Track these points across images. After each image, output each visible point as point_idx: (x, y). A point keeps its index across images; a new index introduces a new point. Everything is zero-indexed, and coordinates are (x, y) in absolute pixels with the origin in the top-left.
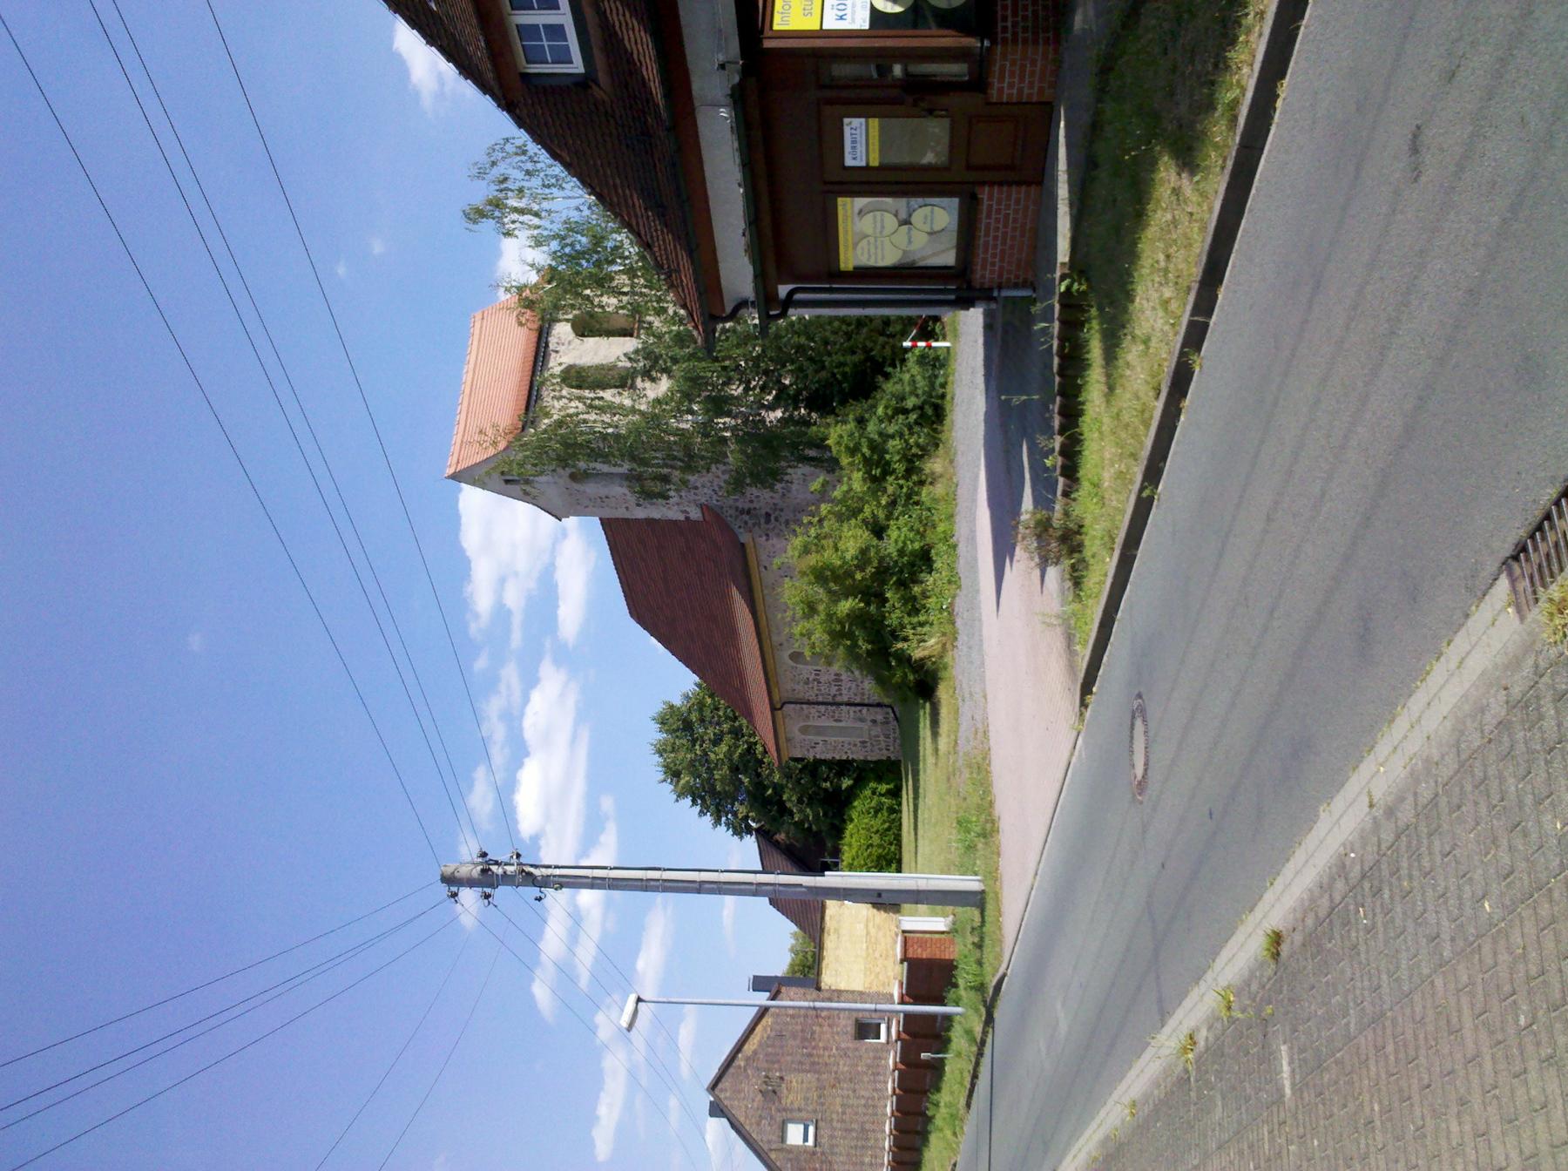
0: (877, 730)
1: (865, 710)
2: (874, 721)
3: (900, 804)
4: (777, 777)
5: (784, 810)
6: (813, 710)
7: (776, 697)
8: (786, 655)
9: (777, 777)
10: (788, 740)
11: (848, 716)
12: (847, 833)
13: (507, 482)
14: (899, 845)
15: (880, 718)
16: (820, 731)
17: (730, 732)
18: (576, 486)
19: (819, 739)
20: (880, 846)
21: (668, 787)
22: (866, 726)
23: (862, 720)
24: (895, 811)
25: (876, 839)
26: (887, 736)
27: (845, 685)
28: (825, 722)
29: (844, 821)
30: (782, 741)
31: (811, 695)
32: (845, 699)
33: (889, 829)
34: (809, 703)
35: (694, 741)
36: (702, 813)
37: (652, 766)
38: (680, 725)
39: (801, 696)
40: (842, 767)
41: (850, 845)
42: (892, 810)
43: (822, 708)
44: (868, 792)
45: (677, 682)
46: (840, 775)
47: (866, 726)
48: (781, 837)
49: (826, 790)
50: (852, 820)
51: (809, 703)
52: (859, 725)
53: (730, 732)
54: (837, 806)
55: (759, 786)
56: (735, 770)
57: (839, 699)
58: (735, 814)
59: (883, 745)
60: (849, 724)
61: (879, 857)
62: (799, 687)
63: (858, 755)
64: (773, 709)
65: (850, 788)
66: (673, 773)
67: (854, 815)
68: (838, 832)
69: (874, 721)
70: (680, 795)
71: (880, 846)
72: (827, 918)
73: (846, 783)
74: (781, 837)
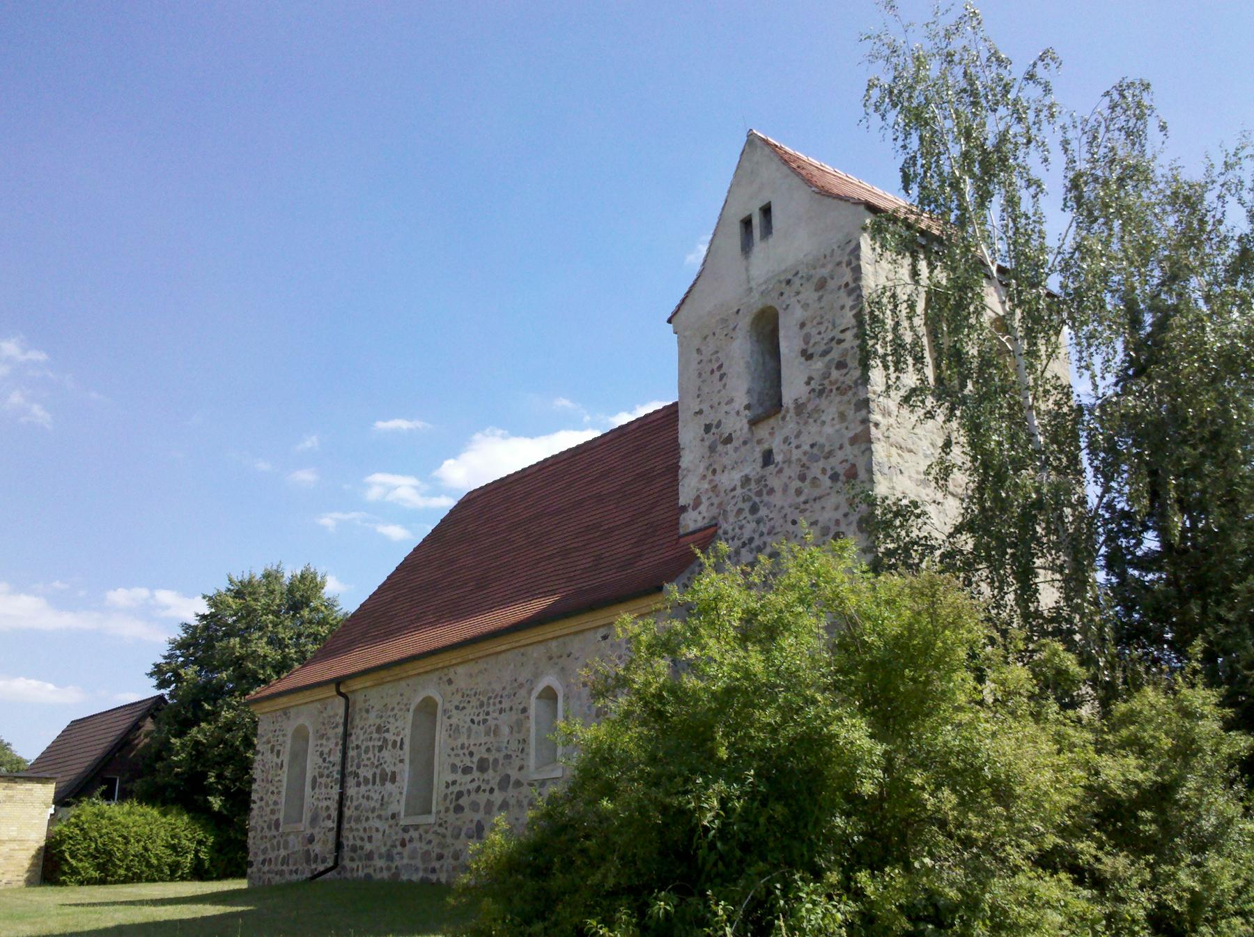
0: (296, 844)
1: (331, 824)
2: (311, 840)
3: (183, 878)
4: (227, 714)
5: (183, 727)
6: (332, 745)
7: (356, 685)
8: (432, 692)
9: (227, 714)
10: (285, 711)
11: (321, 798)
12: (148, 809)
13: (747, 223)
14: (126, 880)
15: (317, 848)
16: (298, 756)
17: (284, 657)
18: (745, 322)
19: (285, 757)
20: (125, 854)
21: (223, 586)
22: (304, 826)
23: (314, 820)
24: (174, 873)
25: (134, 848)
26: (285, 861)
27: (375, 792)
28: (312, 762)
29: (164, 803)
30: (283, 702)
31: (358, 737)
32: (351, 791)
33: (149, 865)
34: (346, 735)
35: (276, 614)
36: (186, 627)
37: (251, 567)
38: (300, 596)
39: (357, 721)
40: (240, 800)
41: (129, 814)
42: (175, 867)
43: (336, 757)
44: (200, 835)
45: (346, 591)
46: (226, 793)
47: (304, 826)
48: (149, 725)
49: (205, 776)
50: (165, 815)
51: (346, 735)
52: (307, 816)
53: (284, 657)
54: (181, 794)
55: (215, 692)
56: (238, 662)
57: (351, 781)
58: (184, 665)
59: (272, 855)
60: (308, 800)
61: (110, 854)
62: (372, 719)
63: (257, 818)
64: (338, 682)
65: (208, 807)
66: (242, 591)
67: (170, 819)
68: (149, 798)
69: (311, 840)
70: (213, 601)
71: (125, 854)
72: (29, 786)
73: (216, 803)
74: (149, 725)
